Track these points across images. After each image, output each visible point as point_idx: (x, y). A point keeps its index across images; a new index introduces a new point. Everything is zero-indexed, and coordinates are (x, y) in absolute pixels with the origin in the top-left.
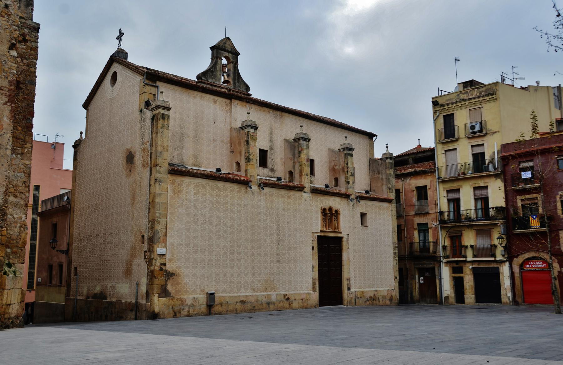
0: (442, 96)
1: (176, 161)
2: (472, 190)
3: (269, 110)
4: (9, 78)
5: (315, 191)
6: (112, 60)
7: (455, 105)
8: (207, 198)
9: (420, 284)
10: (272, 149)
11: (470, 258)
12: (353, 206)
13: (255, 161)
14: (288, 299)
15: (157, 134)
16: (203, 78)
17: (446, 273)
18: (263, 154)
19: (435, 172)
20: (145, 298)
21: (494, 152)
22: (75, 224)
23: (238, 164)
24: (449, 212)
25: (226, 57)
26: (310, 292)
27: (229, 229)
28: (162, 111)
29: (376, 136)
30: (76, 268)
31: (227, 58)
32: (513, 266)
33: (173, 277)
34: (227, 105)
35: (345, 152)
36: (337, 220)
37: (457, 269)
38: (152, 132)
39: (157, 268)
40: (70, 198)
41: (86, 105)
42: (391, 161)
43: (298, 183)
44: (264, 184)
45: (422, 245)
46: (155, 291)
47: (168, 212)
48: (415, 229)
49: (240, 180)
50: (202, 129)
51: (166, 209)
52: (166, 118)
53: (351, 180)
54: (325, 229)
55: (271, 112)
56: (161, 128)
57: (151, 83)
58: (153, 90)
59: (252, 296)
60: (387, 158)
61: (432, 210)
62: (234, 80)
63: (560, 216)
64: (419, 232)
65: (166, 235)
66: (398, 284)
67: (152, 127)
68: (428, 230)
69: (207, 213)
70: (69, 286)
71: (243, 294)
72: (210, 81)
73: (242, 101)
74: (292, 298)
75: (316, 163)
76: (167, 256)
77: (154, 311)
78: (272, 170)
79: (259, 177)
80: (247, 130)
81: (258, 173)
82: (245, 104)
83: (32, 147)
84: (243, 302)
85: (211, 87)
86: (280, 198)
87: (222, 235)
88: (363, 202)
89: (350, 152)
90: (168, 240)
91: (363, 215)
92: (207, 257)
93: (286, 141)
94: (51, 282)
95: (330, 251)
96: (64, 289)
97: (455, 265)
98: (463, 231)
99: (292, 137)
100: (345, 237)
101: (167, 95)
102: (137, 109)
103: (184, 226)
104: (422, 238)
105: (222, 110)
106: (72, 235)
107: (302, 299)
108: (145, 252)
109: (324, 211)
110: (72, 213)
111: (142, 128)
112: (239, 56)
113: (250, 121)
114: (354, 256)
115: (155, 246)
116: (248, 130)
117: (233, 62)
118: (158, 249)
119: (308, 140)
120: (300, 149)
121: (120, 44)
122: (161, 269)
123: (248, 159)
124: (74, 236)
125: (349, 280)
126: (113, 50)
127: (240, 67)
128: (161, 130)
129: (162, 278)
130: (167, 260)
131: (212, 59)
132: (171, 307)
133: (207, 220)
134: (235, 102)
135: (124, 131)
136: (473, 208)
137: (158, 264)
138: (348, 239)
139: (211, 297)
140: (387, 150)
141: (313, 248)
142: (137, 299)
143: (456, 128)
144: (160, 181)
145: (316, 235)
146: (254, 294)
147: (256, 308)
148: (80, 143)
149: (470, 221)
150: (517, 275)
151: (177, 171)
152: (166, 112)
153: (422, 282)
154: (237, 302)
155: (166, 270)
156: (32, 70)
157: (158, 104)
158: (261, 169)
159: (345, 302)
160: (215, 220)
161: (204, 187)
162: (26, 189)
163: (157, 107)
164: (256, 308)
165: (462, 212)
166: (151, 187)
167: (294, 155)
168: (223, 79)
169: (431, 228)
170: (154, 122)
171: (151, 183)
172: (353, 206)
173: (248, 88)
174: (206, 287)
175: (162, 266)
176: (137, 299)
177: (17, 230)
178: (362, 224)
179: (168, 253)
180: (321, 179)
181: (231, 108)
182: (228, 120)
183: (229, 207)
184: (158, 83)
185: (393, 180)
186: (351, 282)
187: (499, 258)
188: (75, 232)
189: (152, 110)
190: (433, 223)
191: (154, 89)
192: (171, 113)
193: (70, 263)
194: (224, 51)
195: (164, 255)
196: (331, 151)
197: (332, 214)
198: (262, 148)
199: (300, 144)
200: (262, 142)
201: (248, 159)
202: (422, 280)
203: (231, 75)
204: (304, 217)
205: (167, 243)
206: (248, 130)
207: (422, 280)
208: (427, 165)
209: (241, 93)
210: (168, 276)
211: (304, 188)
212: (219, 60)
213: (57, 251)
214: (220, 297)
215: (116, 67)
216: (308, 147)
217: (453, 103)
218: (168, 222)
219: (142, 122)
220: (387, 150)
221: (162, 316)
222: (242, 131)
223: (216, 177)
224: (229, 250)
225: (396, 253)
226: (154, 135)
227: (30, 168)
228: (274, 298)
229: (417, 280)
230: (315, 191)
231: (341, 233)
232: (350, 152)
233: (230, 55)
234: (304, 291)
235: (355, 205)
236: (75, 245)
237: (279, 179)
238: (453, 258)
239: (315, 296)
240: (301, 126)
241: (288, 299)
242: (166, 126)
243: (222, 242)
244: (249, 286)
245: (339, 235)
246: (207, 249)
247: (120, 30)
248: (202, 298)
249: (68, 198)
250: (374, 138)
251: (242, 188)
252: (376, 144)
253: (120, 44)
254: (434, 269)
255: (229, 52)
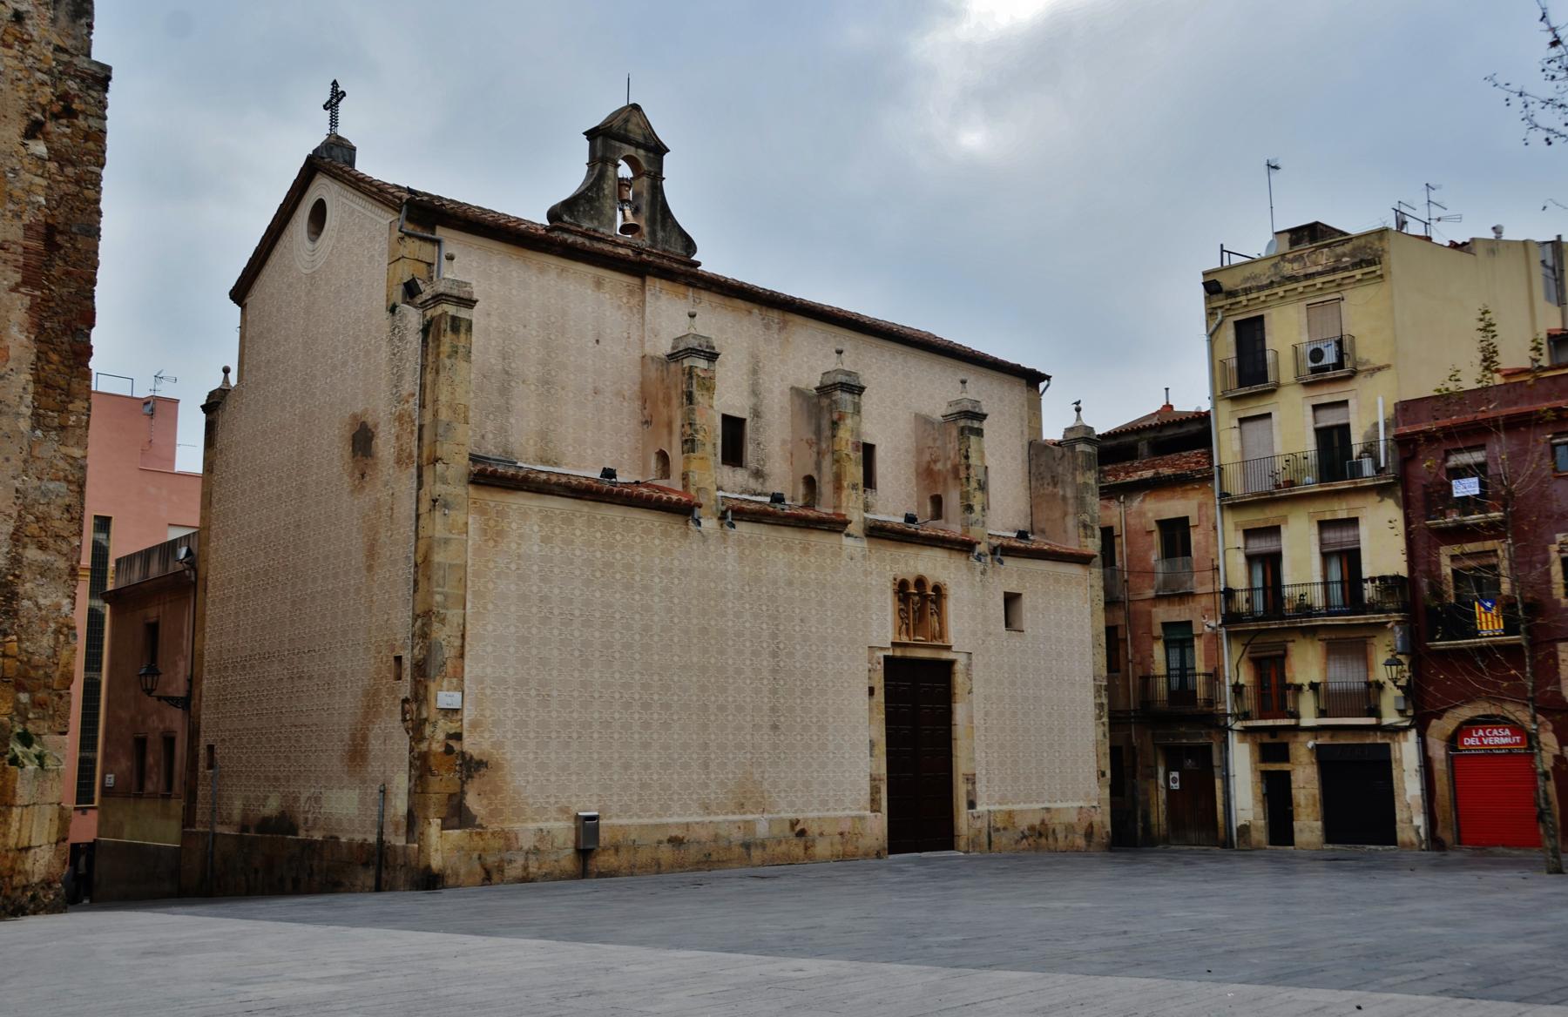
0: (1231, 267)
1: (490, 449)
2: (1315, 530)
3: (749, 305)
4: (27, 219)
5: (878, 532)
6: (313, 167)
7: (1267, 292)
8: (578, 553)
9: (1169, 791)
10: (757, 414)
11: (1309, 719)
12: (983, 573)
13: (709, 448)
14: (802, 833)
15: (437, 373)
16: (566, 218)
17: (1241, 760)
18: (733, 429)
19: (1211, 478)
20: (403, 830)
21: (1376, 425)
22: (208, 623)
23: (663, 457)
24: (1251, 590)
25: (628, 159)
26: (862, 813)
27: (637, 637)
28: (451, 310)
29: (1048, 378)
30: (211, 748)
31: (631, 161)
32: (1430, 740)
33: (483, 770)
34: (631, 293)
35: (962, 423)
36: (940, 613)
37: (1272, 750)
38: (423, 367)
39: (437, 747)
40: (195, 551)
41: (240, 294)
42: (1088, 449)
43: (830, 511)
44: (735, 514)
45: (1175, 682)
46: (432, 811)
47: (469, 592)
48: (1158, 638)
49: (669, 500)
50: (563, 360)
51: (463, 581)
52: (463, 330)
53: (977, 501)
54: (905, 639)
55: (756, 311)
56: (449, 357)
57: (419, 232)
58: (427, 251)
59: (702, 824)
60: (1077, 440)
61: (1202, 584)
62: (652, 222)
63: (1558, 601)
64: (1168, 646)
65: (462, 656)
66: (1108, 791)
67: (424, 354)
68: (1192, 640)
69: (577, 592)
70: (191, 796)
71: (675, 819)
72: (586, 225)
73: (674, 281)
74: (813, 830)
75: (880, 454)
76: (466, 713)
77: (428, 867)
78: (758, 474)
79: (721, 493)
80: (687, 363)
81: (717, 482)
82: (682, 289)
83: (89, 409)
84: (676, 842)
85: (587, 243)
86: (779, 552)
87: (617, 655)
88: (1010, 563)
89: (976, 424)
90: (467, 669)
91: (1011, 600)
92: (575, 715)
93: (797, 392)
94: (141, 786)
95: (918, 699)
96: (177, 806)
97: (1267, 739)
98: (1290, 645)
99: (812, 381)
100: (961, 661)
101: (465, 264)
102: (382, 304)
103: (512, 629)
104: (1175, 664)
105: (619, 307)
106: (202, 656)
107: (841, 834)
108: (405, 701)
109: (902, 588)
110: (200, 594)
111: (396, 356)
112: (666, 157)
113: (695, 336)
114: (987, 714)
115: (432, 686)
116: (690, 362)
117: (648, 174)
118: (441, 695)
119: (858, 390)
120: (835, 416)
121: (334, 122)
122: (449, 750)
123: (690, 444)
124: (206, 658)
125: (971, 779)
126: (314, 139)
127: (668, 187)
128: (448, 362)
129: (451, 775)
130: (465, 726)
131: (591, 164)
132: (475, 855)
133: (577, 613)
134: (654, 284)
135: (345, 364)
136: (1318, 578)
137: (441, 736)
138: (968, 666)
139: (588, 827)
140: (1079, 418)
141: (871, 691)
142: (381, 833)
143: (1270, 356)
144: (446, 506)
145: (881, 654)
146: (707, 819)
147: (714, 857)
148: (223, 397)
149: (1309, 615)
150: (1440, 766)
151: (492, 477)
152: (463, 313)
153: (1176, 786)
154: (660, 842)
155: (463, 754)
156: (90, 194)
157: (441, 290)
158: (727, 470)
159: (962, 843)
160: (598, 615)
161: (568, 521)
162: (74, 527)
163: (438, 298)
164: (714, 857)
165: (1287, 592)
166: (421, 522)
167: (818, 432)
168: (620, 220)
169: (1199, 636)
170: (430, 339)
171: (421, 510)
172: (983, 573)
173: (690, 246)
174: (574, 799)
175: (451, 743)
176: (381, 833)
177: (46, 641)
178: (1008, 624)
179: (467, 705)
180: (895, 499)
181: (644, 301)
182: (635, 336)
183: (637, 578)
184: (441, 232)
185: (1094, 502)
186: (978, 786)
187: (1390, 718)
188: (210, 646)
189: (424, 306)
190: (1206, 621)
191: (428, 247)
192: (475, 315)
193: (194, 734)
194: (625, 141)
195: (456, 710)
196: (923, 421)
197: (924, 597)
198: (731, 413)
199: (835, 402)
200: (729, 396)
201: (690, 444)
202: (1174, 780)
203: (645, 209)
204: (845, 605)
205: (466, 677)
206: (690, 362)
207: (1174, 780)
208: (1188, 461)
209: (670, 259)
210: (469, 770)
211: (846, 523)
212: (611, 168)
213: (159, 698)
214: (612, 827)
215: (323, 188)
216: (857, 410)
217: (1260, 288)
218: (468, 619)
219: (396, 340)
220: (1079, 418)
221: (451, 882)
222: (673, 366)
223: (601, 492)
224: (637, 696)
225: (1101, 705)
226: (429, 377)
227: (83, 468)
228: (762, 830)
229: (1161, 781)
230: (878, 532)
231: (948, 648)
232: (976, 424)
233: (641, 152)
234: (848, 812)
235: (989, 572)
236: (208, 684)
237: (777, 498)
238: (1261, 718)
239: (877, 825)
240: (840, 352)
241: (802, 833)
242: (461, 350)
243: (617, 675)
244: (695, 797)
245: (945, 655)
246: (576, 694)
247: (335, 83)
248: (563, 831)
249: (189, 553)
250: (1042, 385)
251: (673, 525)
252: (1046, 400)
253: (334, 122)
254: (1207, 749)
255: (638, 145)
